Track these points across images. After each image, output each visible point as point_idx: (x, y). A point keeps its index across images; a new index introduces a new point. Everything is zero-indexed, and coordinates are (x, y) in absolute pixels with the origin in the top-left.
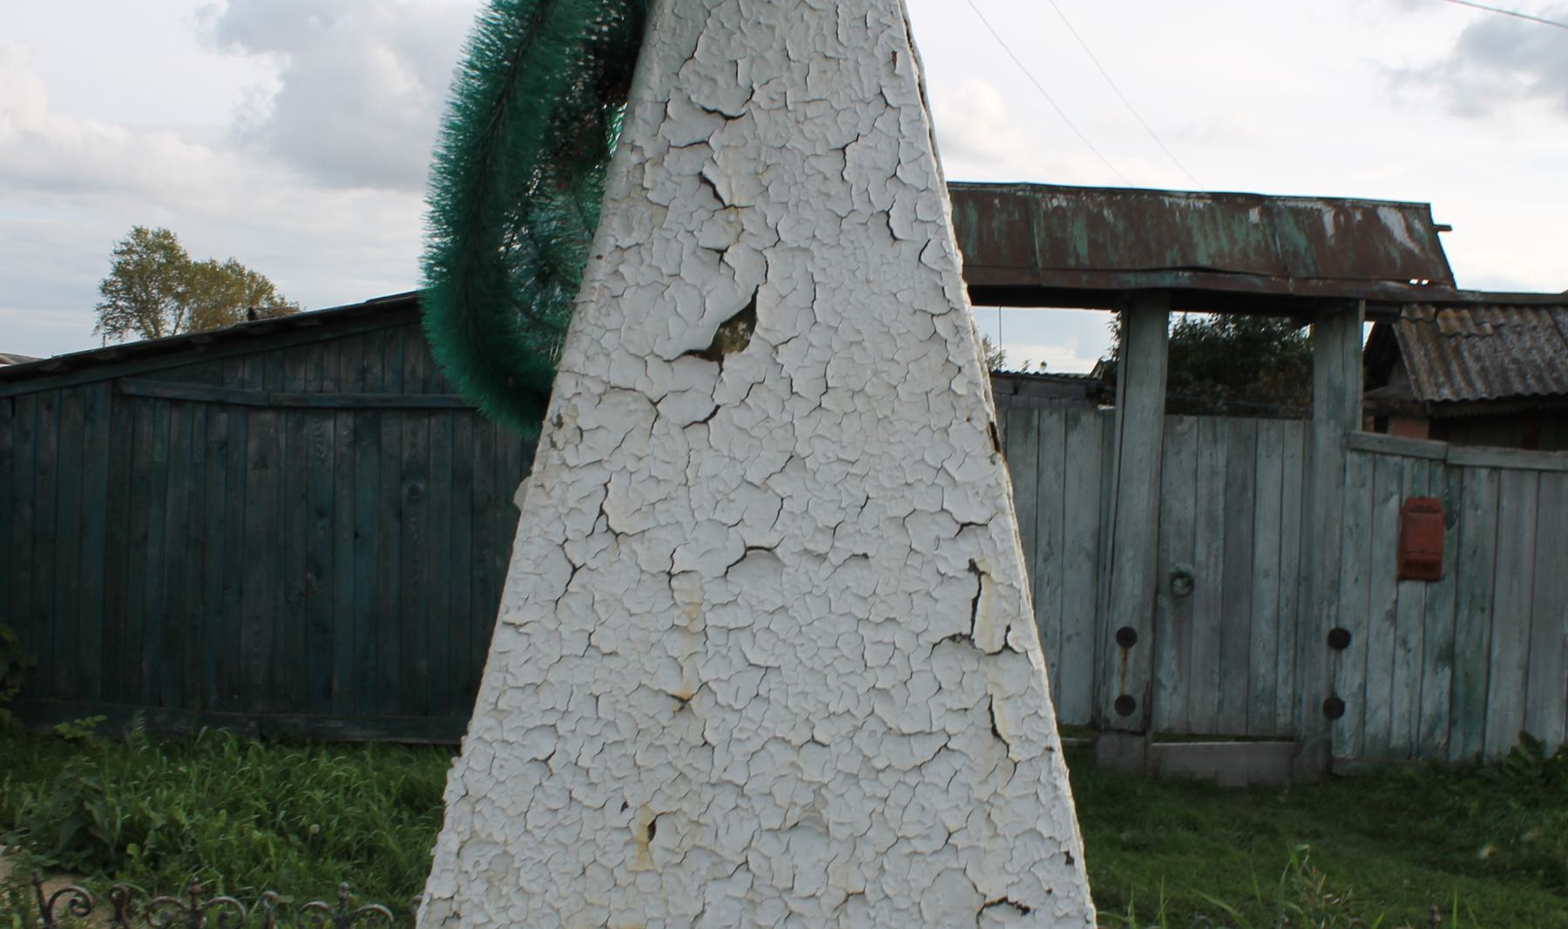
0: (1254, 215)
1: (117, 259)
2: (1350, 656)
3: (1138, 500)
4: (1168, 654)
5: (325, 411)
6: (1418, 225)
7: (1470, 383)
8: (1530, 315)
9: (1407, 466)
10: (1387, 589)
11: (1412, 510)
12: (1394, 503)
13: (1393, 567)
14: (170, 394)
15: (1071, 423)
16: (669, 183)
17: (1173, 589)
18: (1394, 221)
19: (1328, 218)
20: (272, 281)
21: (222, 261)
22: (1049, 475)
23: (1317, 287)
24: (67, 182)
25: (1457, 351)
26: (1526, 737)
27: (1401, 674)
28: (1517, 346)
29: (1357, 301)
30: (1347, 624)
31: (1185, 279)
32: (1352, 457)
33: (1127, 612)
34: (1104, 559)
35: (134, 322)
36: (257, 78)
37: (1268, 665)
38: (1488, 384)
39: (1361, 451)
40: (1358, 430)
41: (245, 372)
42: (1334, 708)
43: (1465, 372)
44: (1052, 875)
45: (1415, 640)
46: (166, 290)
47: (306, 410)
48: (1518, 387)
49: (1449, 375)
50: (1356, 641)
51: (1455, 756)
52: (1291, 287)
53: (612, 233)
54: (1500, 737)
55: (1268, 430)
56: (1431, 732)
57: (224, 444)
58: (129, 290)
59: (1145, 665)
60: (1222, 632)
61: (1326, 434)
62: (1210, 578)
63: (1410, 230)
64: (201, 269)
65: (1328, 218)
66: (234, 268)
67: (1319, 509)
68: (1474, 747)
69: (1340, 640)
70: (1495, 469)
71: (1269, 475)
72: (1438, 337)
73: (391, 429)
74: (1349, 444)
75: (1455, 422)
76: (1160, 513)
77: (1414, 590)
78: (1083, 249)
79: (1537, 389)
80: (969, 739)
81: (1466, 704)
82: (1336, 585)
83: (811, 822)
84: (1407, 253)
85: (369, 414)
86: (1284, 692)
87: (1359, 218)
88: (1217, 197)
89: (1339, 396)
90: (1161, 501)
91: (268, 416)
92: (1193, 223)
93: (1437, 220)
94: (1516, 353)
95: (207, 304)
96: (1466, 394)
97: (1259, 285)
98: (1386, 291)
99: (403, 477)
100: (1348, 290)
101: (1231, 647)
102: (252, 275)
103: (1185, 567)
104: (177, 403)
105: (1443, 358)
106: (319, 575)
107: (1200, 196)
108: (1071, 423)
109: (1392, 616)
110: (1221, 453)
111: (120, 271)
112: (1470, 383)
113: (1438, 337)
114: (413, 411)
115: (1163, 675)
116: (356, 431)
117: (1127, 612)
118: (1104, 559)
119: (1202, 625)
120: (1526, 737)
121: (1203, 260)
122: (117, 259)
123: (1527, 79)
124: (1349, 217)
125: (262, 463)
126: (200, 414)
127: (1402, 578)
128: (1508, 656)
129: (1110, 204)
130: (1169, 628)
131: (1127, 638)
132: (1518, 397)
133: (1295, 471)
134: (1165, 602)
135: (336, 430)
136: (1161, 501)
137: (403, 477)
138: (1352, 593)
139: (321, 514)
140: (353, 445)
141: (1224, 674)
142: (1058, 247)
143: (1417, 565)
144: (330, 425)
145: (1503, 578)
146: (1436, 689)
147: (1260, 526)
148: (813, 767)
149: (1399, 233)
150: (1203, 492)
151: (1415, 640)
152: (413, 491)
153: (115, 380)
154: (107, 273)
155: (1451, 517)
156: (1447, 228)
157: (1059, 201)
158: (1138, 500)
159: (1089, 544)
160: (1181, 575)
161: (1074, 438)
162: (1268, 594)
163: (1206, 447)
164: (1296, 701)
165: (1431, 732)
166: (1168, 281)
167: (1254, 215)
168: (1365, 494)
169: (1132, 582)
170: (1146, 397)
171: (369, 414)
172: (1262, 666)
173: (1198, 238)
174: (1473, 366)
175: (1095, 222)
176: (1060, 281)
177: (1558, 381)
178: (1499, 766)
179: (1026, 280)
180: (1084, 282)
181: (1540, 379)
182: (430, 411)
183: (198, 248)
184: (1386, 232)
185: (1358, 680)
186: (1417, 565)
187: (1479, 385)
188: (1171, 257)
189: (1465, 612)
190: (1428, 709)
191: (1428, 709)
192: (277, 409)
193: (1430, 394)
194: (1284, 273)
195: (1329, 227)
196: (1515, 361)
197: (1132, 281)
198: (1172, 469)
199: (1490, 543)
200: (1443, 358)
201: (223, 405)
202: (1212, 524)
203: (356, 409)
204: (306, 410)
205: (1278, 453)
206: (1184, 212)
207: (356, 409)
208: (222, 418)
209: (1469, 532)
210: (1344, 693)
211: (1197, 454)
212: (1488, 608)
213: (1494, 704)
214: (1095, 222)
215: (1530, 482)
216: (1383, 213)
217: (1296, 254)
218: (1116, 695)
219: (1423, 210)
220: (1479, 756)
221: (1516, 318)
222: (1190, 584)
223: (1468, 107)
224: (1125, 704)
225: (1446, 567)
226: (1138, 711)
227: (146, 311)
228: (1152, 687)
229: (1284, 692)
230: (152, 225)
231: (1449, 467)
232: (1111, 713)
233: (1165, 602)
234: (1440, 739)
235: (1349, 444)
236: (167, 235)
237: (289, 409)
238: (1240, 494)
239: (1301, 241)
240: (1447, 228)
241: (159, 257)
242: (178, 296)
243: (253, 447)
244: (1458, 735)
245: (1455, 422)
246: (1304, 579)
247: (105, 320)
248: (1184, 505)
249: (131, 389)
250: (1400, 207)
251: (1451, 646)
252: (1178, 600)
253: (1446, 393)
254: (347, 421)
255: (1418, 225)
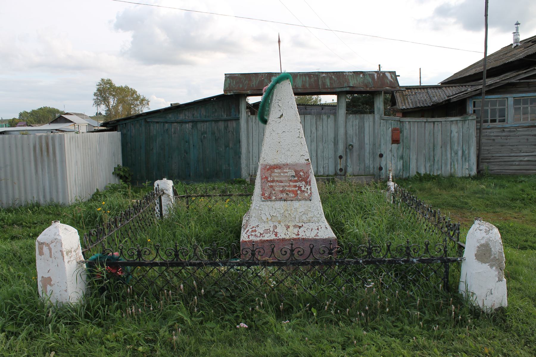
0: (361, 75)
1: (98, 87)
2: (383, 159)
3: (342, 131)
4: (349, 160)
5: (186, 123)
6: (393, 76)
7: (409, 105)
8: (422, 90)
9: (393, 122)
10: (389, 145)
11: (394, 130)
12: (390, 129)
13: (391, 141)
14: (156, 121)
15: (328, 117)
16: (276, 105)
17: (349, 148)
18: (388, 75)
19: (376, 75)
20: (136, 90)
21: (124, 86)
22: (325, 127)
23: (373, 89)
24: (80, 67)
25: (407, 98)
26: (417, 173)
27: (393, 162)
28: (419, 97)
29: (381, 92)
30: (382, 153)
31: (348, 89)
32: (382, 121)
33: (340, 152)
34: (336, 143)
35: (103, 103)
36: (126, 38)
37: (368, 161)
38: (413, 105)
39: (384, 120)
40: (383, 116)
41: (170, 116)
42: (381, 169)
43: (408, 103)
44: (306, 153)
45: (395, 155)
46: (111, 94)
47: (183, 122)
48: (419, 105)
49: (405, 104)
50: (384, 156)
51: (404, 177)
52: (368, 89)
53: (272, 109)
54: (413, 172)
55: (366, 116)
56: (399, 172)
57: (167, 130)
58: (101, 94)
59: (344, 162)
60: (359, 155)
61: (377, 116)
62: (356, 145)
63: (391, 77)
64: (119, 88)
65: (376, 75)
66: (127, 87)
67: (376, 131)
68: (408, 175)
69: (381, 156)
70: (409, 122)
71: (366, 125)
72: (403, 95)
73: (199, 125)
74: (381, 118)
75: (406, 113)
76: (346, 133)
77: (395, 146)
78: (329, 84)
79: (422, 105)
80: (299, 144)
81: (406, 167)
82: (380, 145)
83: (289, 150)
84: (391, 81)
85: (195, 123)
86: (371, 166)
87: (381, 75)
88: (354, 72)
89: (379, 109)
90: (346, 131)
91: (175, 124)
92: (350, 78)
93: (397, 74)
94: (419, 98)
95: (121, 97)
96: (408, 107)
97: (362, 89)
98: (386, 89)
99: (202, 134)
100: (379, 89)
101: (361, 158)
102: (131, 89)
103: (351, 143)
104: (157, 122)
105: (404, 100)
106: (187, 154)
107: (351, 72)
108: (328, 117)
109: (391, 151)
110: (357, 121)
111: (98, 90)
112: (409, 105)
113: (403, 95)
114: (203, 121)
115: (348, 164)
116: (193, 126)
117: (340, 152)
118: (336, 143)
119: (355, 154)
120: (417, 173)
121: (351, 85)
122: (98, 87)
123: (452, 20)
124: (380, 75)
125: (175, 133)
126: (162, 124)
127: (392, 143)
128: (413, 157)
129: (334, 75)
130: (349, 155)
131: (341, 157)
132: (418, 107)
133: (371, 124)
134: (348, 150)
135: (188, 126)
136: (346, 131)
137: (202, 134)
138: (383, 147)
139: (187, 142)
140: (192, 129)
141: (360, 163)
142: (324, 84)
143: (395, 141)
144: (187, 125)
145: (412, 143)
146: (400, 164)
147: (365, 135)
148: (289, 146)
149: (389, 77)
150: (354, 129)
151: (395, 155)
152: (204, 137)
153: (145, 119)
154: (95, 90)
155: (401, 131)
156: (399, 76)
157: (324, 75)
158: (342, 131)
159: (333, 140)
160: (351, 145)
161: (329, 120)
162: (367, 147)
163: (355, 120)
164: (374, 168)
165: (399, 172)
166: (345, 89)
167: (361, 75)
168: (385, 128)
169: (341, 146)
170: (342, 111)
171: (195, 123)
172: (367, 161)
173: (350, 81)
174: (410, 101)
175: (331, 79)
176: (324, 91)
177: (427, 104)
178: (412, 178)
179: (318, 91)
180: (329, 90)
181: (423, 103)
182: (206, 121)
183: (117, 83)
184: (387, 77)
185: (385, 163)
186: (395, 141)
187: (411, 105)
188: (346, 85)
189: (405, 149)
190: (398, 168)
191: (398, 168)
192: (177, 122)
193: (401, 107)
194: (367, 87)
195: (376, 78)
196: (418, 100)
197: (338, 90)
198: (347, 125)
199: (409, 136)
200: (404, 100)
201: (167, 122)
202: (356, 135)
203: (192, 122)
204: (183, 122)
205: (368, 120)
206: (348, 76)
207: (192, 122)
208: (167, 125)
209: (405, 134)
210: (382, 166)
211: (353, 122)
212: (409, 148)
213: (411, 167)
214: (331, 79)
215: (416, 124)
216: (386, 74)
217: (369, 83)
218: (339, 168)
219: (394, 73)
220: (409, 177)
221: (419, 91)
222: (352, 147)
223: (437, 28)
224: (341, 170)
225: (401, 141)
226: (344, 171)
227: (105, 100)
228: (346, 166)
229: (371, 166)
230: (106, 78)
231: (401, 122)
232: (338, 172)
233: (348, 150)
234: (401, 174)
235: (381, 118)
236: (109, 80)
237: (179, 122)
238: (361, 129)
239: (370, 80)
240: (399, 76)
241: (108, 86)
242: (113, 95)
243: (173, 130)
244: (404, 173)
245: (406, 113)
246: (374, 145)
247: (96, 102)
248: (350, 132)
249: (149, 120)
250: (390, 72)
251: (403, 156)
252: (350, 150)
253: (404, 107)
254: (191, 124)
255: (393, 76)
